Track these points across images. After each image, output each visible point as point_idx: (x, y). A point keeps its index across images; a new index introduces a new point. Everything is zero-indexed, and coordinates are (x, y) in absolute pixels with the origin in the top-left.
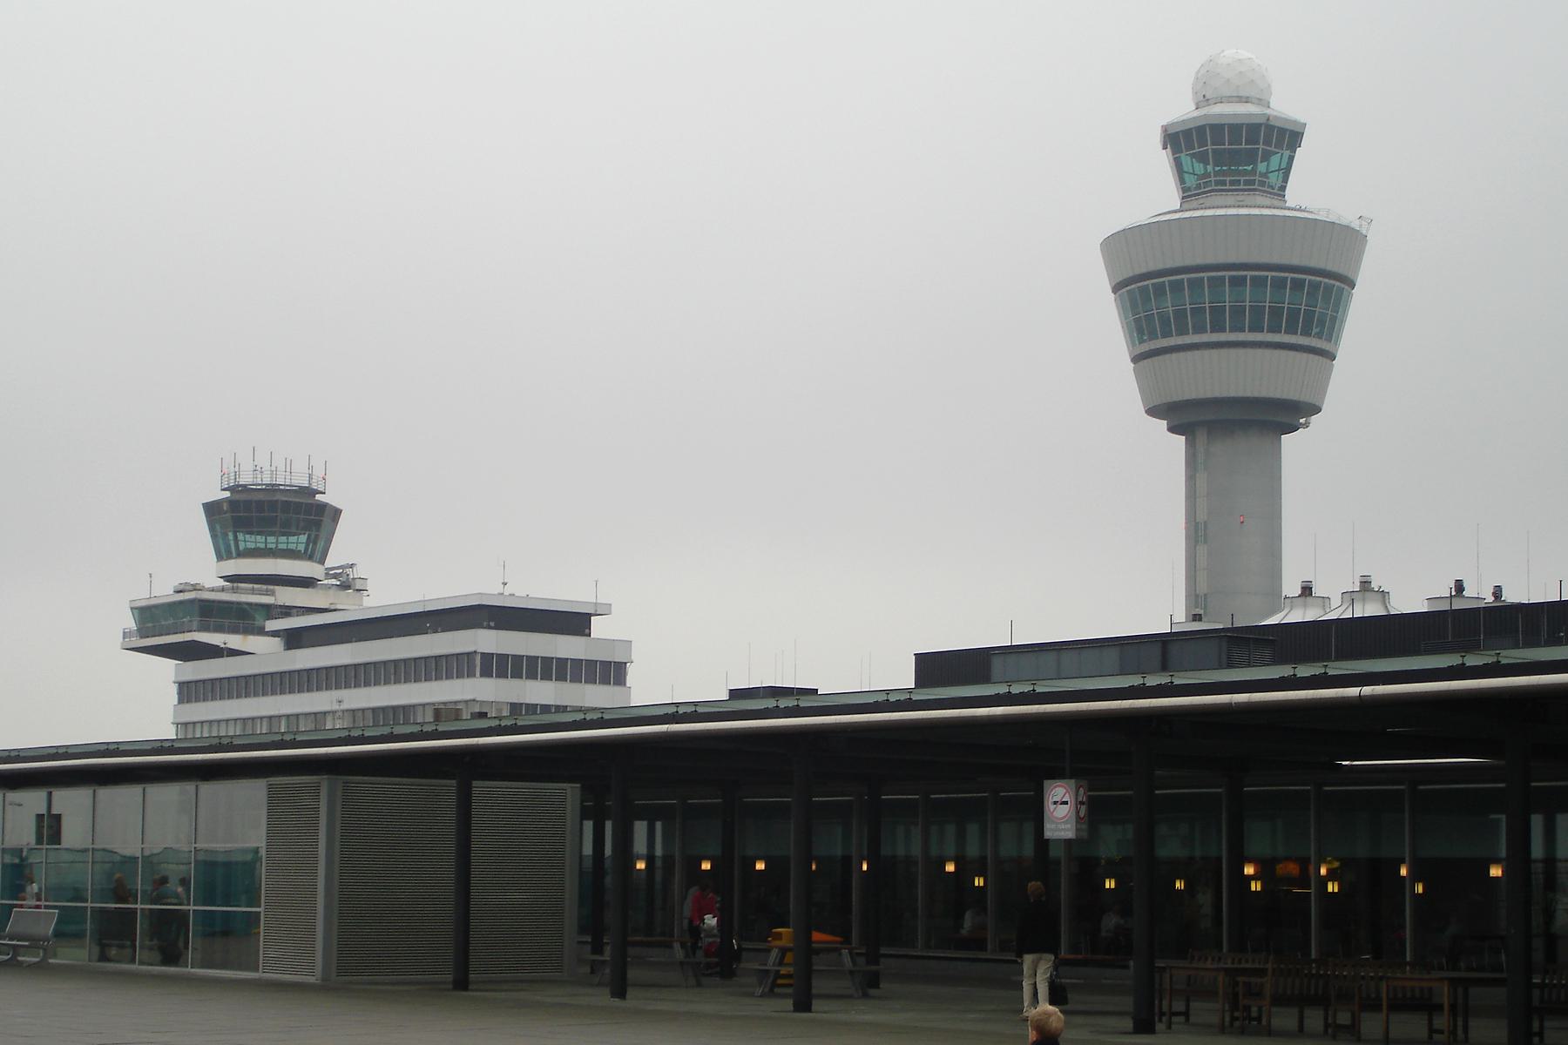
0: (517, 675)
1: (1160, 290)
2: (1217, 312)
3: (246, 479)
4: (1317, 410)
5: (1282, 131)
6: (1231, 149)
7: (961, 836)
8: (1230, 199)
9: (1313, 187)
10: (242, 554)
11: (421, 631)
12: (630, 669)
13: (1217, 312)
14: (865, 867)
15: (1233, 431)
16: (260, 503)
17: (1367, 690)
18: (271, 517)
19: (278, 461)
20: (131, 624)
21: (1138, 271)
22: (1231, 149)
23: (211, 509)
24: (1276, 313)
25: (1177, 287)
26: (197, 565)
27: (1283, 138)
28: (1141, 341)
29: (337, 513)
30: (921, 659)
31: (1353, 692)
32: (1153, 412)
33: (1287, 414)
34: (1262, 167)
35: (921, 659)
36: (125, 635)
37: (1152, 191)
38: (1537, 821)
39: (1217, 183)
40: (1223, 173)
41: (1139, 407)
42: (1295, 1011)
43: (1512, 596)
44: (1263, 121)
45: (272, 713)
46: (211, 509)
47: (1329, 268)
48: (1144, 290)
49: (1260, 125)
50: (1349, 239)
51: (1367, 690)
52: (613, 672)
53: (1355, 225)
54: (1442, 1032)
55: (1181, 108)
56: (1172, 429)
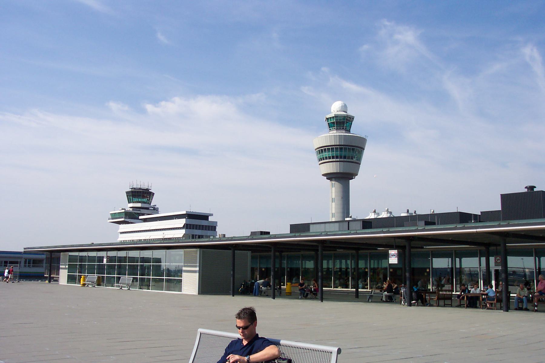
0: (193, 229)
9: (356, 130)
12: (217, 227)
15: (343, 178)
16: (138, 192)
17: (478, 230)
19: (141, 183)
23: (127, 193)
29: (154, 194)
30: (292, 226)
31: (475, 230)
33: (351, 176)
35: (292, 226)
38: (458, 260)
42: (443, 301)
43: (418, 213)
46: (127, 193)
48: (322, 150)
50: (363, 141)
51: (478, 230)
52: (213, 227)
54: (249, 316)
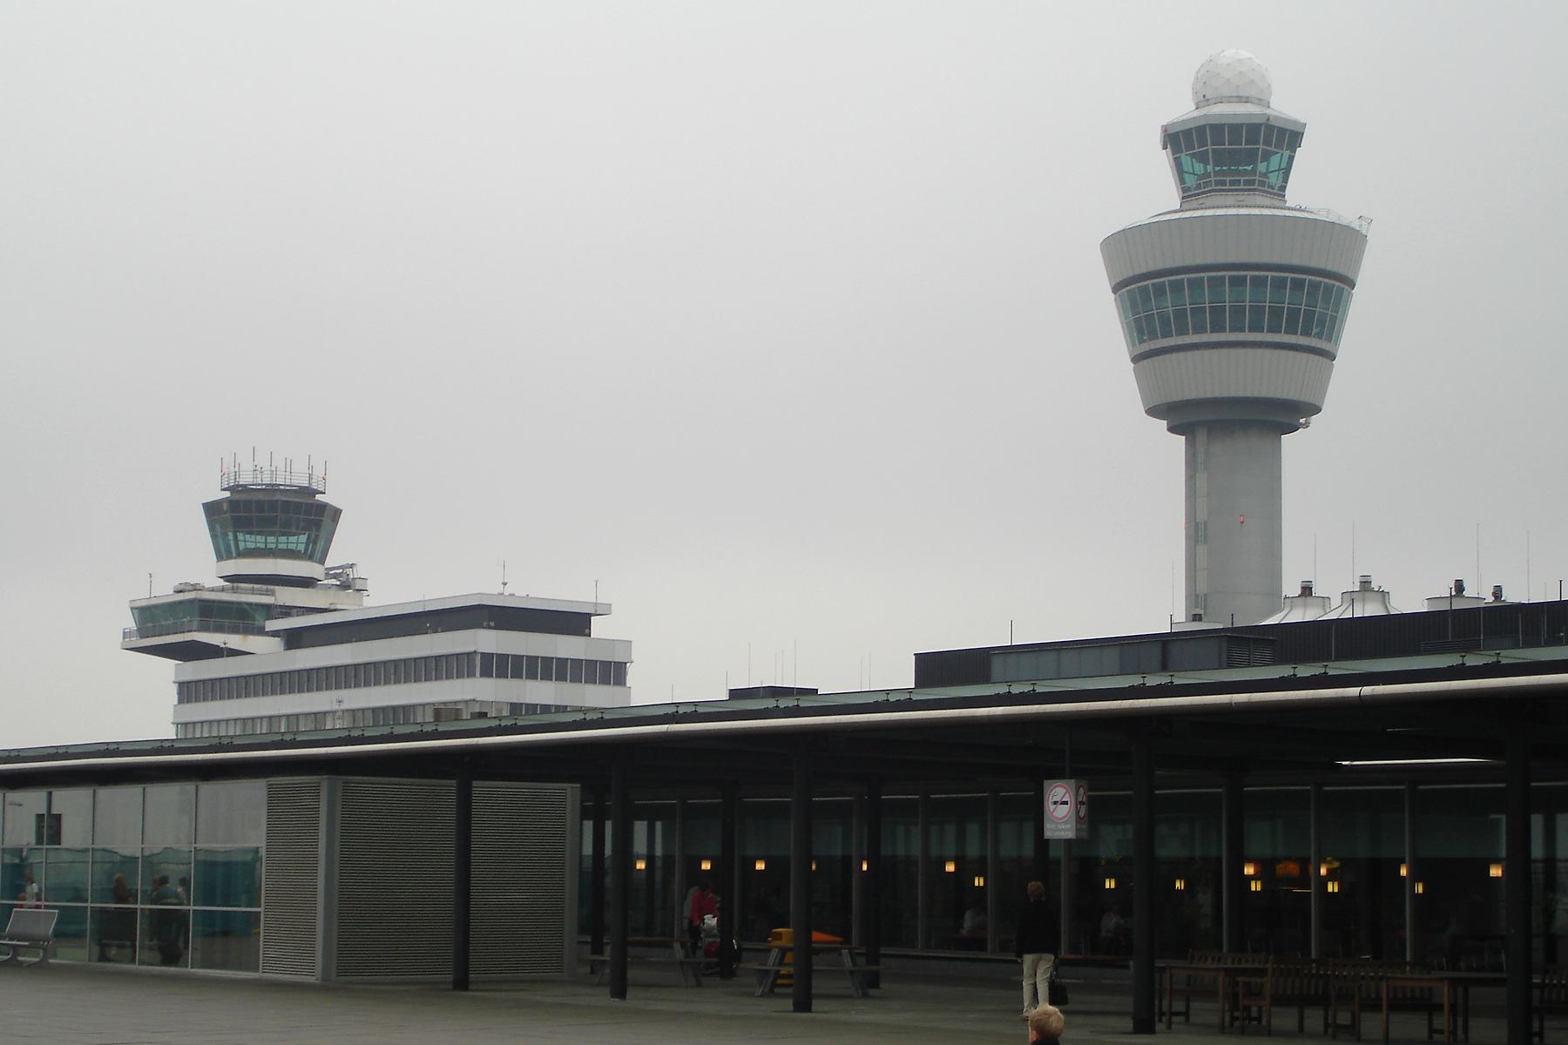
0: (517, 675)
1: (1160, 290)
2: (1217, 312)
3: (246, 479)
4: (1317, 410)
5: (1282, 131)
6: (1231, 149)
7: (961, 836)
8: (1230, 199)
9: (1313, 187)
10: (242, 554)
11: (421, 631)
12: (630, 669)
13: (1217, 312)
14: (865, 867)
15: (1233, 431)
16: (260, 503)
17: (1367, 690)
18: (271, 517)
19: (278, 461)
20: (131, 624)
21: (1138, 271)
22: (1231, 149)
23: (211, 509)
24: (1276, 313)
25: (1177, 287)
26: (197, 565)
27: (1283, 138)
28: (1141, 341)
29: (337, 513)
30: (921, 659)
31: (1353, 692)
32: (1153, 412)
33: (1287, 414)
34: (1262, 167)
35: (921, 659)
36: (125, 635)
37: (1152, 191)
38: (1537, 821)
39: (1217, 183)
40: (1223, 173)
41: (1139, 407)
42: (1295, 1011)
43: (1512, 596)
44: (1263, 121)
45: (272, 713)
46: (211, 509)
47: (1329, 268)
48: (1144, 290)
49: (1260, 125)
50: (1349, 239)
51: (1367, 690)
52: (613, 672)
53: (1355, 225)
54: (1442, 1032)
55: (1181, 108)
56: (1172, 429)
